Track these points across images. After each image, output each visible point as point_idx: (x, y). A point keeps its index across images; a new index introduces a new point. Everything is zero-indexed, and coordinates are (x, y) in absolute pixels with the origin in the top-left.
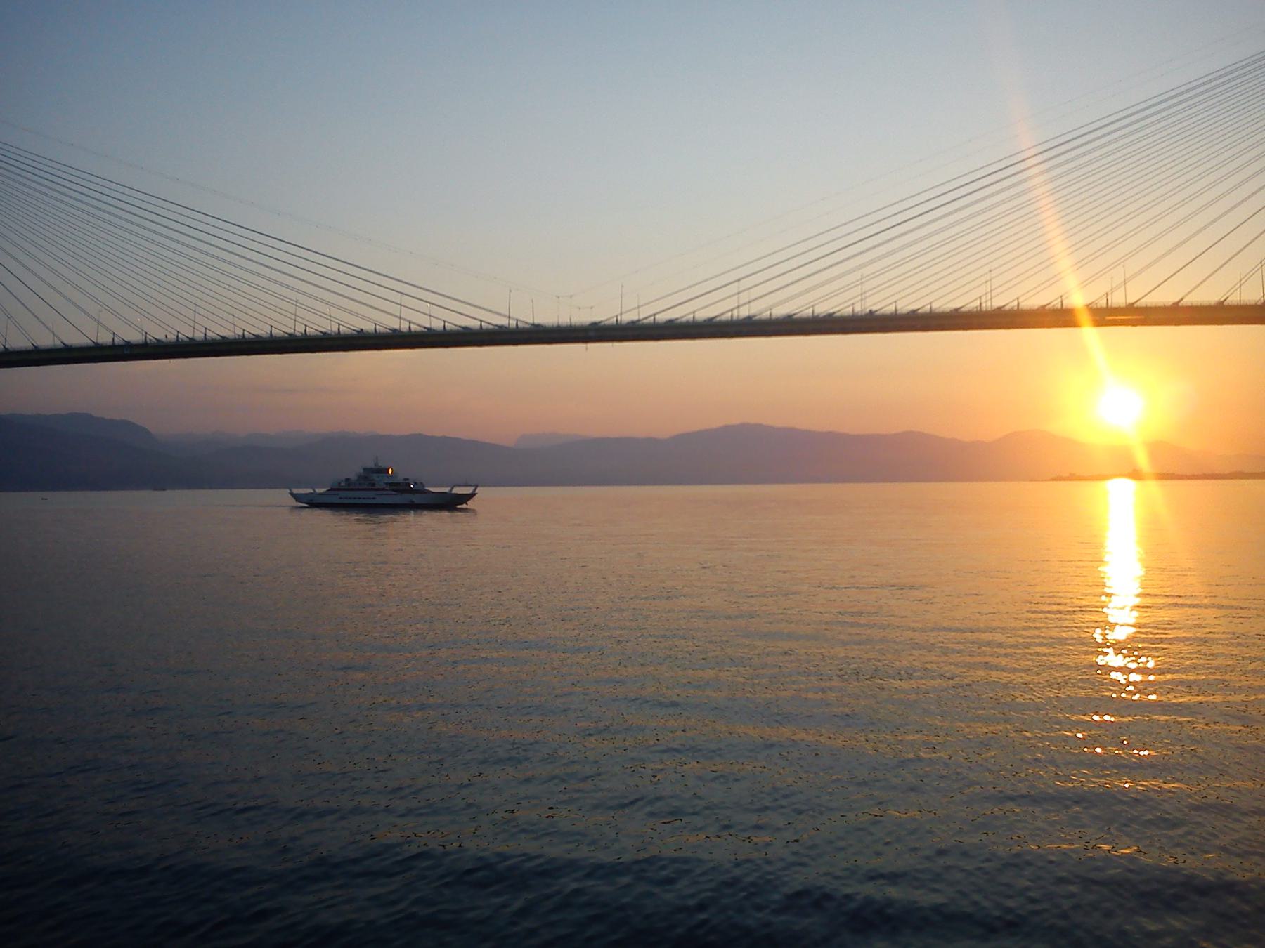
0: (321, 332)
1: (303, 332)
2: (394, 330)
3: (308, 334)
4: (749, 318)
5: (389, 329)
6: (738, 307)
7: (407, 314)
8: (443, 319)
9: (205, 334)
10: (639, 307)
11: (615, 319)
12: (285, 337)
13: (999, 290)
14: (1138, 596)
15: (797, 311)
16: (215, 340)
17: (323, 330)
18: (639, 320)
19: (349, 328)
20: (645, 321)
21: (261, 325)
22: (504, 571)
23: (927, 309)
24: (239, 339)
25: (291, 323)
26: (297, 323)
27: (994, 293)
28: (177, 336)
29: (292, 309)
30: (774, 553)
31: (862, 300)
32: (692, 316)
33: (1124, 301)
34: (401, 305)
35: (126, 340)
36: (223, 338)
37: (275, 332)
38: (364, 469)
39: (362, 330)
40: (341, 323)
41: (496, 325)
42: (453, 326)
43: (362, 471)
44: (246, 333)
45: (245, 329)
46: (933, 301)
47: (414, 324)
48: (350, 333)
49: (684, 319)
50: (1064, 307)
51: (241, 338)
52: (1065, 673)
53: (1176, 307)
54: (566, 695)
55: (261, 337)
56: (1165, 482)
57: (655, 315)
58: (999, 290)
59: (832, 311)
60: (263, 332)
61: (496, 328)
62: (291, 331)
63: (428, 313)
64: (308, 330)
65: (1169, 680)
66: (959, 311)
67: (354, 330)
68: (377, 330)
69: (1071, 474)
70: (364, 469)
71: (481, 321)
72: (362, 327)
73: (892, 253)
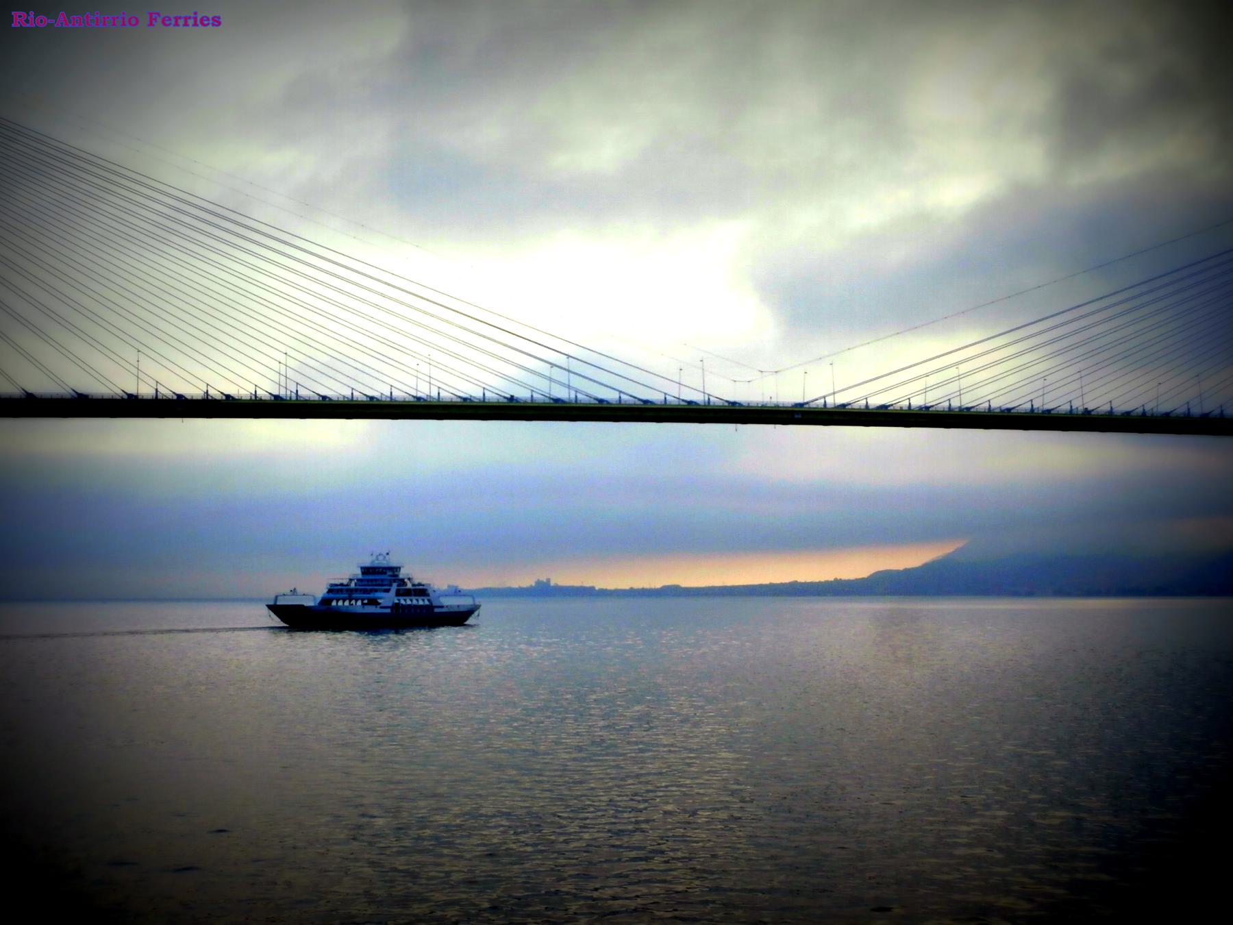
0: (460, 397)
1: (389, 394)
2: (130, 396)
7: (577, 382)
8: (352, 386)
9: (157, 390)
10: (834, 393)
13: (922, 392)
15: (893, 403)
17: (371, 393)
19: (497, 394)
25: (411, 381)
26: (432, 386)
31: (960, 395)
32: (822, 401)
33: (833, 401)
34: (569, 371)
37: (396, 394)
38: (363, 568)
39: (512, 396)
43: (359, 572)
44: (668, 397)
45: (354, 388)
47: (581, 392)
48: (721, 404)
49: (897, 407)
51: (987, 411)
56: (440, 605)
58: (922, 392)
59: (1009, 406)
60: (335, 393)
61: (726, 404)
63: (571, 375)
64: (355, 394)
65: (447, 733)
66: (1052, 412)
68: (486, 398)
70: (363, 568)
71: (620, 392)
72: (512, 394)
73: (329, 286)
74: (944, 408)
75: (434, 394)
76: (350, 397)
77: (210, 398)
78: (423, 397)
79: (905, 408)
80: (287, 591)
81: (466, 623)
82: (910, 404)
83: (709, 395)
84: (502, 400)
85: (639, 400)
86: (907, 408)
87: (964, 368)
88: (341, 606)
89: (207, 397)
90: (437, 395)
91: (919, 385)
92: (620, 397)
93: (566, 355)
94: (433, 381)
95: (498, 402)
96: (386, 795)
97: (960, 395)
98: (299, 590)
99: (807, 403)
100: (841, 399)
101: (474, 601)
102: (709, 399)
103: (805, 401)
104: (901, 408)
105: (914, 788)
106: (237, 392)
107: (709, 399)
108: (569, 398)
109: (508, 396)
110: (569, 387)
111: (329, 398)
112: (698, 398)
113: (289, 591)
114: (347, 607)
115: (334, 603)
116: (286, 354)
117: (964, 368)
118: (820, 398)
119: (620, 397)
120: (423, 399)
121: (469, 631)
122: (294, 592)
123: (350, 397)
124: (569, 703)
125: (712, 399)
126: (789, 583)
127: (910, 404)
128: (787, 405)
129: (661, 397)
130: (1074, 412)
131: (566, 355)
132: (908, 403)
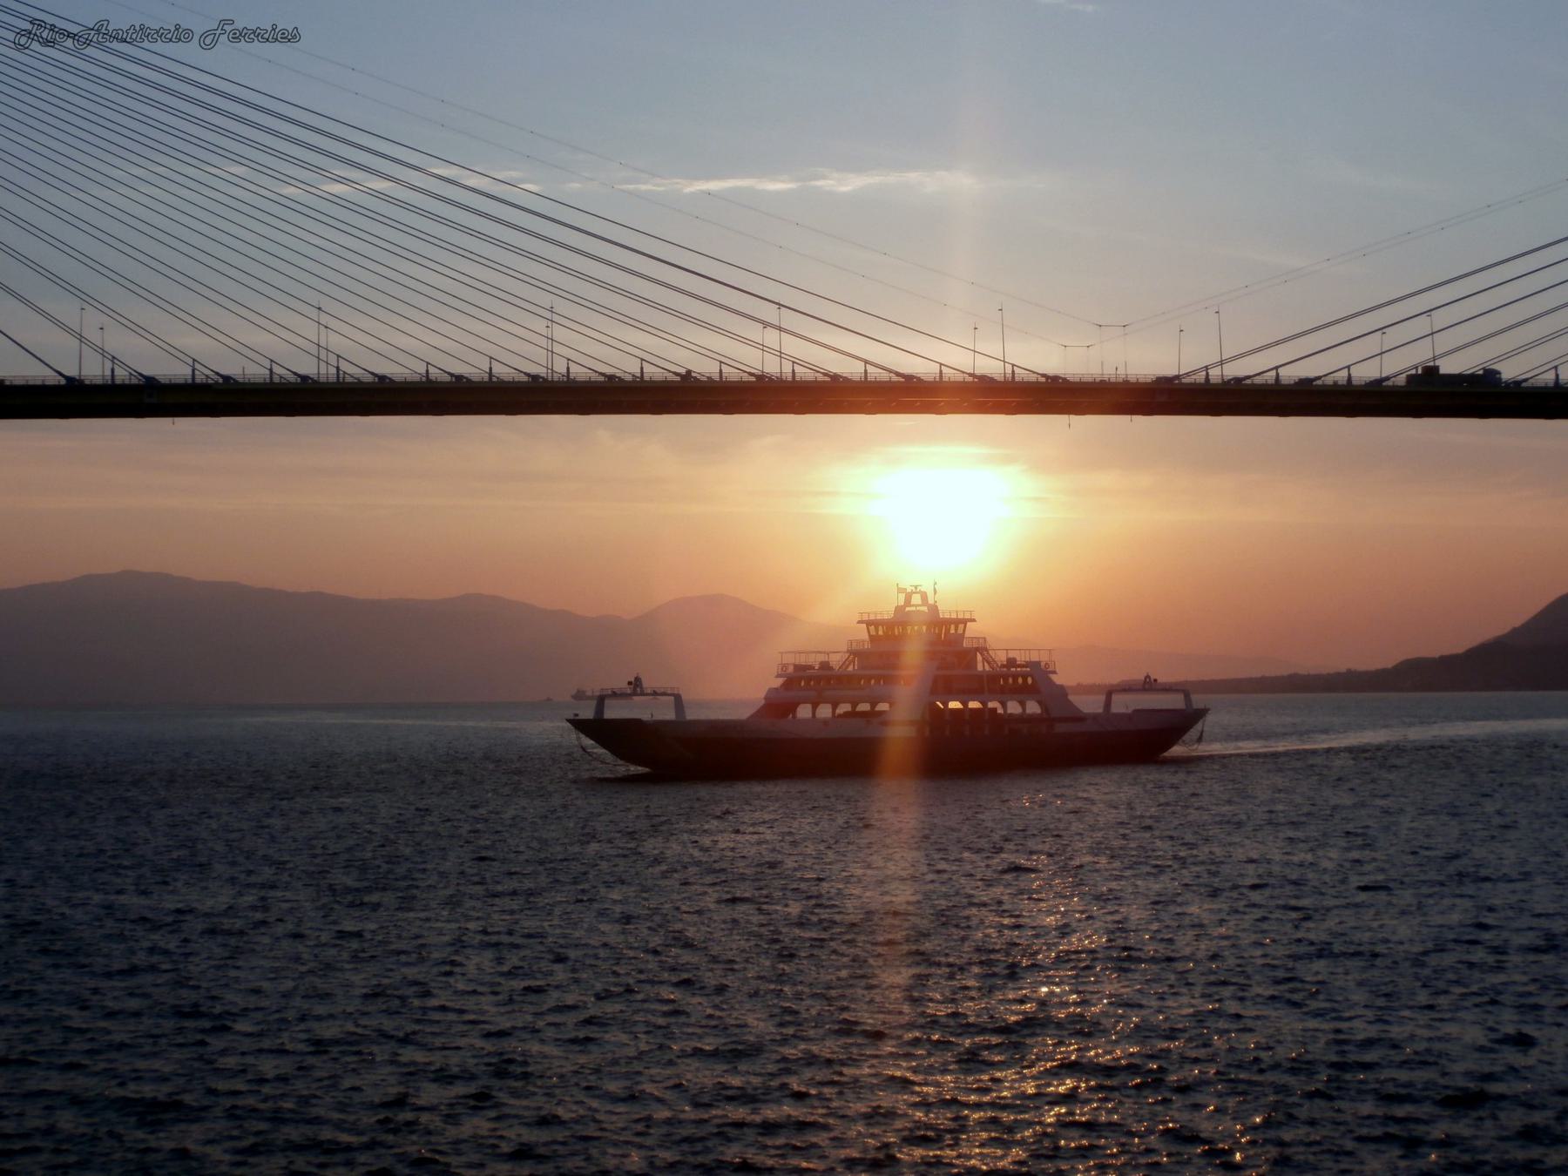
1: (564, 371)
4: (1379, 382)
5: (825, 374)
7: (793, 346)
11: (1204, 373)
16: (360, 382)
18: (1177, 377)
20: (1258, 380)
22: (556, 801)
23: (1341, 377)
24: (634, 381)
27: (550, 353)
28: (271, 370)
29: (540, 325)
30: (1255, 1013)
32: (1344, 373)
35: (145, 373)
36: (382, 378)
37: (499, 370)
39: (689, 372)
40: (723, 359)
41: (1043, 375)
42: (594, 374)
44: (945, 370)
46: (1281, 366)
48: (812, 379)
49: (1329, 381)
50: (798, 379)
53: (1305, 385)
55: (469, 380)
57: (1276, 368)
60: (407, 371)
62: (541, 371)
69: (578, 691)
71: (866, 362)
75: (560, 367)
76: (637, 371)
77: (494, 379)
78: (542, 375)
79: (1271, 381)
80: (621, 684)
81: (1177, 750)
82: (1349, 375)
83: (1013, 365)
84: (746, 378)
85: (898, 374)
87: (1442, 317)
88: (805, 721)
90: (565, 371)
94: (557, 348)
95: (590, 382)
98: (647, 684)
99: (1387, 378)
100: (1234, 370)
101: (1024, 709)
102: (1013, 371)
103: (1384, 375)
105: (466, 758)
106: (188, 371)
107: (1013, 371)
108: (103, 376)
109: (683, 371)
111: (466, 378)
113: (625, 685)
114: (825, 722)
115: (804, 712)
116: (319, 309)
117: (1442, 317)
118: (1272, 369)
120: (312, 379)
121: (1167, 776)
122: (636, 684)
123: (637, 371)
125: (1017, 370)
127: (1349, 375)
128: (257, 381)
129: (935, 368)
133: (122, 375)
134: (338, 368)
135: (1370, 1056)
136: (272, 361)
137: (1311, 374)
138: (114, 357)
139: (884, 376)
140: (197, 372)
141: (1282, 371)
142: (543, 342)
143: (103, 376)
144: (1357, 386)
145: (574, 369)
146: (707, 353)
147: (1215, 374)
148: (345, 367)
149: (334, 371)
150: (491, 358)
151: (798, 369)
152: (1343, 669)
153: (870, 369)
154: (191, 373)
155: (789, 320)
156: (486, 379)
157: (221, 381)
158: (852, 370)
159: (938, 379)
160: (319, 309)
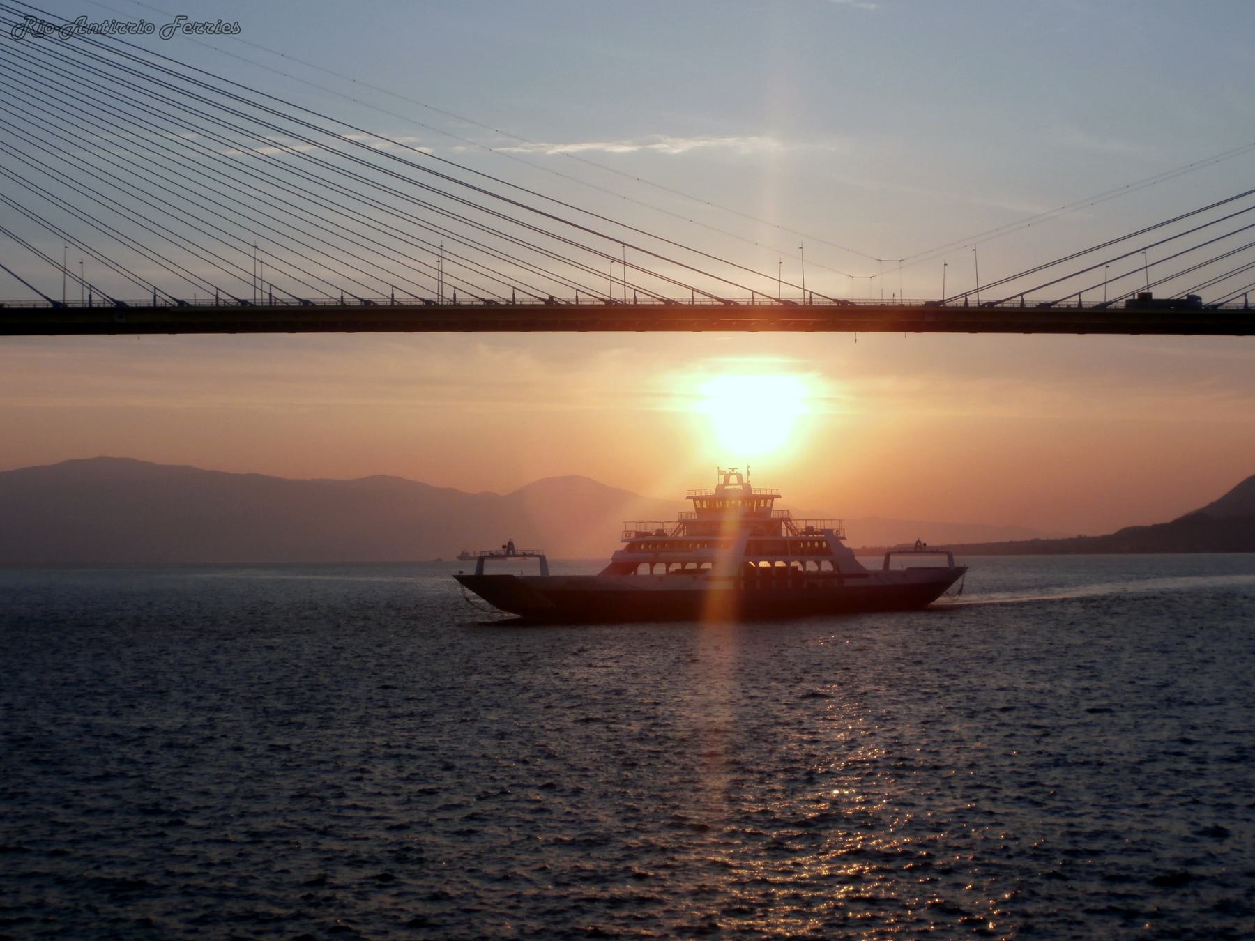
3: (458, 301)
4: (1104, 306)
6: (978, 290)
7: (635, 277)
11: (964, 298)
12: (542, 305)
14: (464, 580)
16: (288, 306)
18: (942, 302)
20: (1007, 304)
21: (422, 279)
23: (1074, 301)
25: (433, 285)
28: (217, 296)
29: (432, 260)
32: (1076, 299)
36: (306, 302)
37: (399, 296)
39: (551, 298)
40: (579, 288)
41: (835, 300)
49: (1064, 305)
50: (638, 303)
52: (899, 792)
54: (254, 797)
55: (852, 304)
57: (1022, 294)
60: (325, 297)
62: (433, 297)
67: (601, 299)
71: (693, 290)
74: (149, 304)
75: (448, 294)
76: (510, 297)
77: (396, 304)
79: (1018, 305)
80: (497, 547)
82: (1080, 300)
85: (718, 299)
86: (1077, 306)
87: (1154, 254)
89: (217, 303)
91: (1098, 276)
92: (693, 297)
93: (622, 243)
94: (446, 279)
96: (533, 807)
97: (442, 282)
98: (518, 548)
99: (1111, 303)
100: (987, 296)
102: (811, 297)
103: (1107, 300)
104: (1069, 306)
106: (151, 297)
107: (811, 297)
109: (547, 297)
110: (625, 284)
111: (373, 303)
112: (246, 294)
116: (256, 247)
117: (1154, 254)
118: (1018, 295)
119: (693, 297)
120: (250, 303)
122: (509, 547)
123: (510, 297)
124: (477, 692)
125: (814, 296)
126: (1118, 534)
127: (1080, 300)
130: (628, 303)
131: (622, 243)
132: (1078, 300)
133: (97, 300)
134: (270, 295)
135: (1097, 845)
136: (217, 289)
137: (1049, 299)
138: (91, 286)
139: (707, 301)
140: (157, 298)
141: (1026, 297)
142: (435, 274)
143: (83, 301)
144: (1086, 309)
145: (460, 295)
146: (565, 282)
147: (972, 299)
148: (276, 293)
149: (267, 297)
150: (393, 286)
151: (639, 295)
152: (1075, 535)
153: (697, 295)
154: (152, 298)
155: (631, 256)
156: (389, 303)
157: (177, 304)
158: (682, 296)
159: (750, 303)
160: (256, 247)
